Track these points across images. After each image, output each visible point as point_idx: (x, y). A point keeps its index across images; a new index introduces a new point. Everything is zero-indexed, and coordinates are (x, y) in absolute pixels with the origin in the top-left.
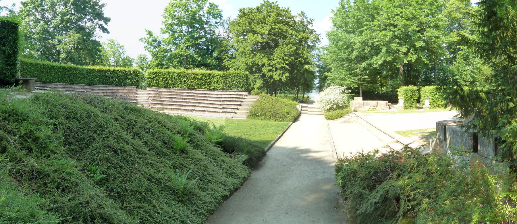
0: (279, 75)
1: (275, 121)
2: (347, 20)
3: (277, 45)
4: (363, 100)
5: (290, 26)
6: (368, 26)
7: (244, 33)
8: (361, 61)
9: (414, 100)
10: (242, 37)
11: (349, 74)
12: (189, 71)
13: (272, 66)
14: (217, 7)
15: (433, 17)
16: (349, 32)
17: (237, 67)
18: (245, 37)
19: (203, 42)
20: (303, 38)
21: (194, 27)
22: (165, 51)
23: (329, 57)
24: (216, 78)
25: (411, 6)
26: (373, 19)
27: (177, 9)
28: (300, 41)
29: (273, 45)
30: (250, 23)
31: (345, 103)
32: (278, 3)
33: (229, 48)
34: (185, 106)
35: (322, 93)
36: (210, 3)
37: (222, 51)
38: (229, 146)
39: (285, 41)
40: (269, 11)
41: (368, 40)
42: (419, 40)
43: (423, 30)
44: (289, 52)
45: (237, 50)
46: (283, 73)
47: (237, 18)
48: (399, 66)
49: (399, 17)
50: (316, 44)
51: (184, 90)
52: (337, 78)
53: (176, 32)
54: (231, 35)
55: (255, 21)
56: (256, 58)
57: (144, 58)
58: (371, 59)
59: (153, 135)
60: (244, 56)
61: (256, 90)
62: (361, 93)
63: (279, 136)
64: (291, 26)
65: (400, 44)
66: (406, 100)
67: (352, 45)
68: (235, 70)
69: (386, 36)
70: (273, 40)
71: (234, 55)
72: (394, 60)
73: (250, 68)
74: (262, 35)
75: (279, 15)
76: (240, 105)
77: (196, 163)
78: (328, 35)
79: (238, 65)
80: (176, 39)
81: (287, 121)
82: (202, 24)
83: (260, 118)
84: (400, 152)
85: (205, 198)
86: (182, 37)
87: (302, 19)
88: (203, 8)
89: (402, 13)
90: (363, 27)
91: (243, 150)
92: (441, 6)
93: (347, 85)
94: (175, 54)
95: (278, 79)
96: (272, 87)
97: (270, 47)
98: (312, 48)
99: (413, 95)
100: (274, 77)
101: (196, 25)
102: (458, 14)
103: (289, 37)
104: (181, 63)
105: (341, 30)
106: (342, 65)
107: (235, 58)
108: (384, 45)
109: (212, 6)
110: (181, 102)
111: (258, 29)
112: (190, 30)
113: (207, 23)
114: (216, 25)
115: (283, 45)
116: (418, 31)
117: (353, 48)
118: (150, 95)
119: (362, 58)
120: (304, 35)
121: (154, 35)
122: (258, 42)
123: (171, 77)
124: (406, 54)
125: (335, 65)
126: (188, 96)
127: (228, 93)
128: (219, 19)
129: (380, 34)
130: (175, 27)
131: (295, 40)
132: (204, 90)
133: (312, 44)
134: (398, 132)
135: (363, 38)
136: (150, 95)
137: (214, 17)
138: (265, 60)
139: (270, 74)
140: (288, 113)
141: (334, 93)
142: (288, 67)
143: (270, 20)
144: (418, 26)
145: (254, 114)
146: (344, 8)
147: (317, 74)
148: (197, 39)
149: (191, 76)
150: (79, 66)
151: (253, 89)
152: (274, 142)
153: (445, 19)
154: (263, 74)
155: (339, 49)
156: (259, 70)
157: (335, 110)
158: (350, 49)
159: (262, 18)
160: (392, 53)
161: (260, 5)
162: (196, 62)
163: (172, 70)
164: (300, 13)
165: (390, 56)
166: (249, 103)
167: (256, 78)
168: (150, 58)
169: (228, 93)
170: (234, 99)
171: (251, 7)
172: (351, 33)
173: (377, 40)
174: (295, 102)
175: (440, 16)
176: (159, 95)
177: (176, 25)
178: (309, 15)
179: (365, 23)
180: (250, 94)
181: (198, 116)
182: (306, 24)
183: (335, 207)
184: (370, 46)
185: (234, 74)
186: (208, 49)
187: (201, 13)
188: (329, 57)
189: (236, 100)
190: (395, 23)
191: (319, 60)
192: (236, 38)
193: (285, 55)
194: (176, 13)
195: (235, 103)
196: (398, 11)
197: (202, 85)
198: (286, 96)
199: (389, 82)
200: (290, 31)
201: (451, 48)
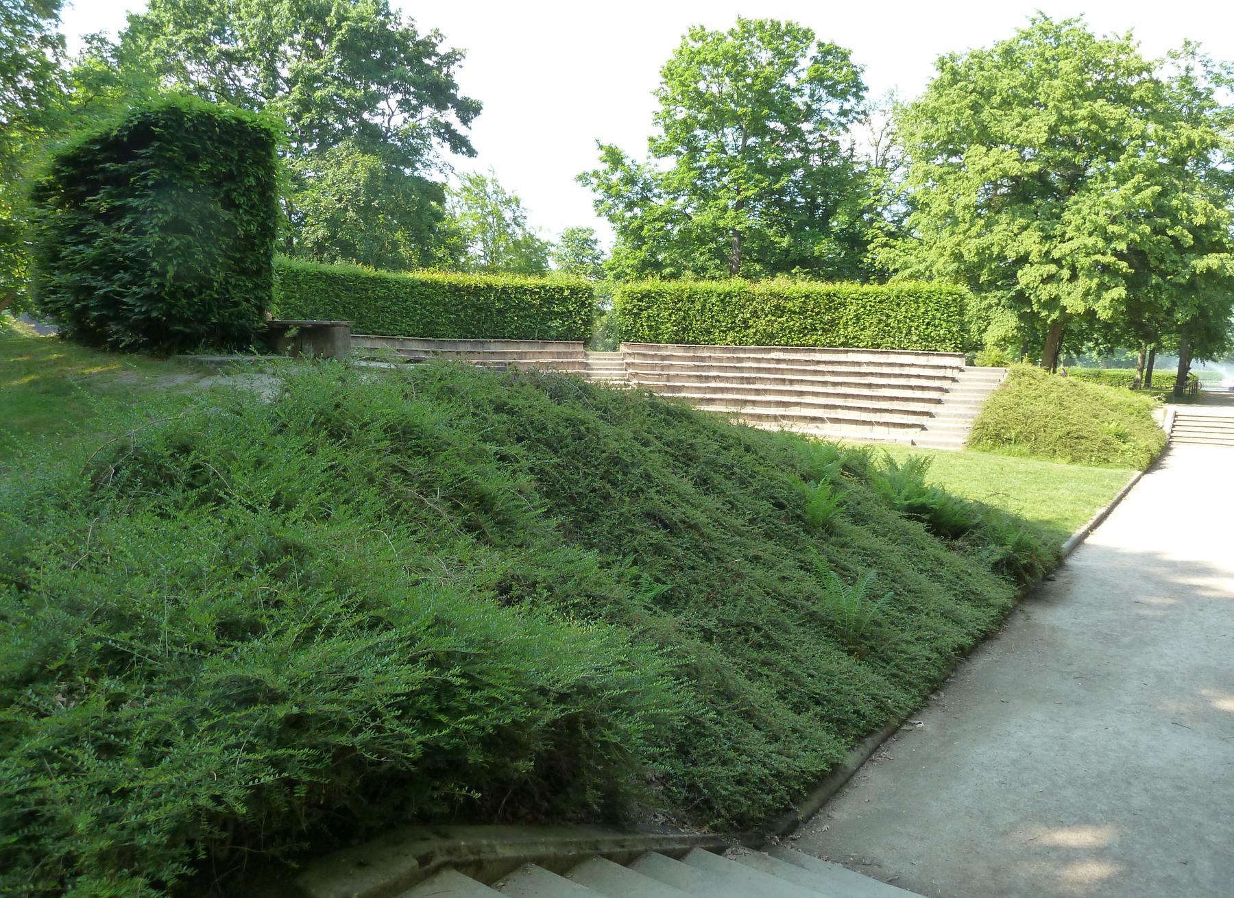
0: (1086, 294)
1: (1074, 461)
3: (1076, 181)
7: (952, 146)
12: (763, 286)
13: (1058, 262)
14: (845, 57)
22: (668, 217)
24: (853, 308)
30: (976, 108)
32: (1084, 19)
34: (754, 403)
36: (821, 45)
38: (948, 523)
46: (1103, 287)
51: (745, 351)
56: (997, 236)
57: (586, 240)
59: (743, 483)
63: (1100, 511)
64: (1141, 102)
75: (1090, 63)
76: (939, 402)
79: (924, 261)
80: (701, 176)
81: (1123, 465)
83: (1016, 448)
85: (912, 649)
86: (725, 167)
87: (1188, 69)
88: (795, 64)
94: (703, 227)
95: (1081, 310)
100: (1065, 301)
101: (772, 125)
104: (724, 259)
109: (828, 52)
110: (738, 391)
111: (1006, 126)
113: (809, 113)
114: (843, 120)
115: (1105, 180)
118: (630, 371)
120: (1196, 135)
121: (627, 162)
123: (698, 306)
126: (759, 370)
127: (781, 355)
128: (853, 101)
130: (699, 132)
136: (630, 371)
137: (833, 92)
138: (1030, 242)
139: (1046, 292)
140: (1122, 437)
142: (1123, 265)
145: (992, 435)
148: (776, 173)
149: (766, 301)
150: (383, 273)
151: (978, 346)
159: (1023, 85)
161: (1015, 35)
164: (1178, 47)
166: (972, 397)
167: (990, 306)
168: (607, 239)
169: (893, 358)
170: (914, 382)
174: (1144, 398)
176: (663, 368)
177: (703, 127)
182: (1201, 84)
185: (915, 296)
193: (1114, 220)
194: (702, 86)
197: (803, 331)
200: (1137, 126)
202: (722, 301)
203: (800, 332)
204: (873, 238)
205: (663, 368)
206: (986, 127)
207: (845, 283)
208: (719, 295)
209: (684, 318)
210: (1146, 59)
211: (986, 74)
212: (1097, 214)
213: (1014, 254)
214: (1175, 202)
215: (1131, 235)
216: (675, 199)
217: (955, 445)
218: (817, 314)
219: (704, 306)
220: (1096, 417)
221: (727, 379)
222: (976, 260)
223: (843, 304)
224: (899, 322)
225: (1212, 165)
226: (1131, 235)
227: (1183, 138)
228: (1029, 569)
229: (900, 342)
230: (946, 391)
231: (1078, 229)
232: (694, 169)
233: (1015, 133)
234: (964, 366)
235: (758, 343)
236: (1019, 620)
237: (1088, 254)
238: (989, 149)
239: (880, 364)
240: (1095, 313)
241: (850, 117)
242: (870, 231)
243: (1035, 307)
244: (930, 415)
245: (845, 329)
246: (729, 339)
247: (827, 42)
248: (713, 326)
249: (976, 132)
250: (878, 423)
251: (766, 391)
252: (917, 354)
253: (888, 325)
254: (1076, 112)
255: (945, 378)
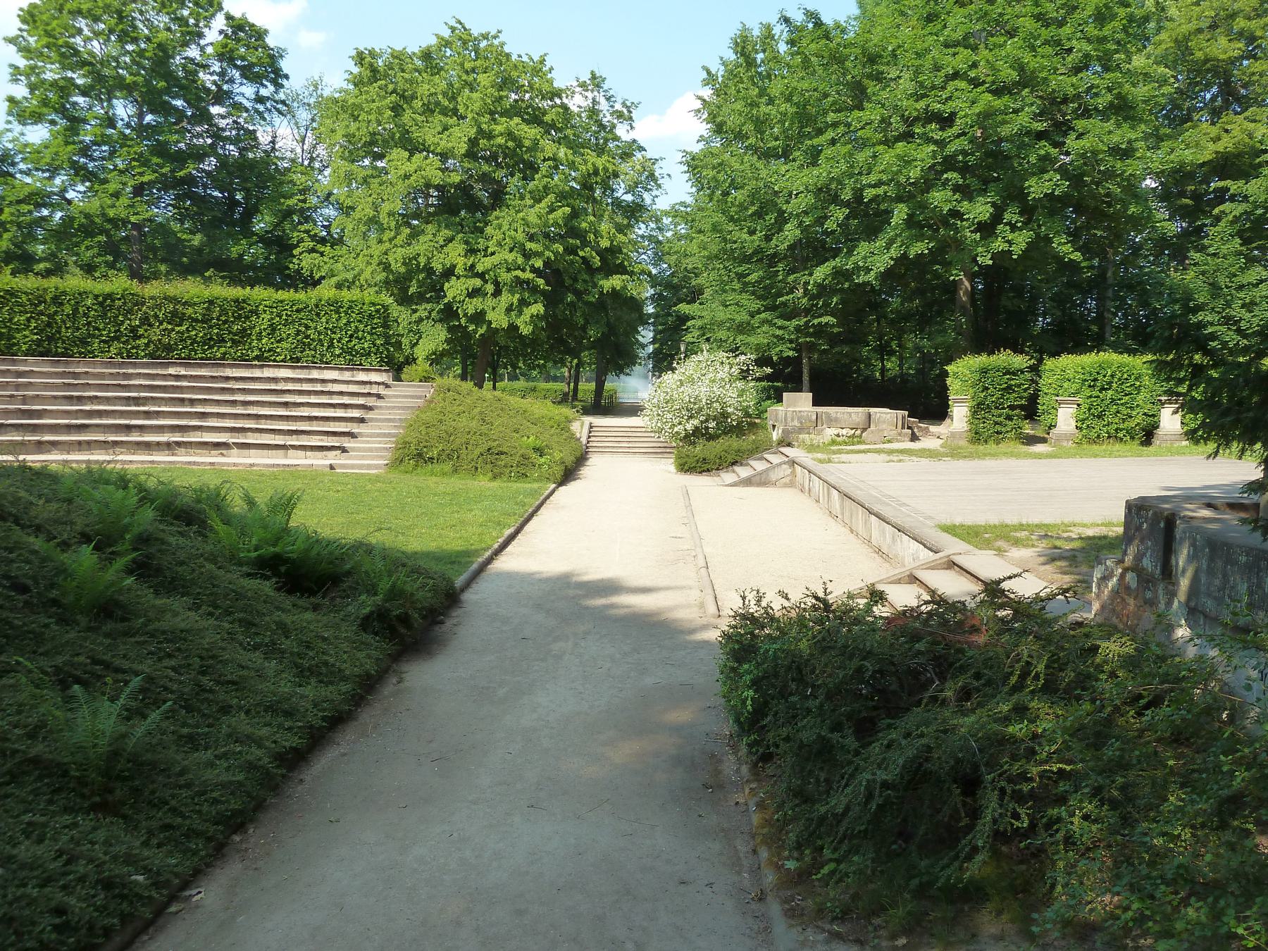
0: (509, 310)
2: (764, 109)
3: (498, 197)
4: (815, 404)
5: (548, 127)
6: (841, 129)
7: (374, 147)
8: (807, 259)
9: (1012, 408)
10: (367, 162)
11: (767, 309)
12: (152, 289)
13: (482, 276)
15: (1107, 69)
16: (767, 155)
17: (350, 276)
18: (379, 164)
19: (209, 173)
20: (596, 173)
21: (166, 109)
22: (38, 199)
23: (693, 247)
25: (1011, 34)
26: (859, 96)
27: (82, 23)
28: (587, 186)
29: (484, 196)
31: (747, 415)
32: (502, 38)
33: (313, 200)
35: (668, 377)
36: (229, 17)
37: (288, 213)
38: (308, 573)
39: (532, 185)
40: (468, 65)
41: (840, 182)
42: (1044, 171)
43: (1063, 128)
44: (546, 225)
45: (346, 210)
46: (523, 303)
47: (345, 85)
48: (957, 275)
49: (962, 84)
50: (646, 196)
51: (135, 365)
52: (721, 324)
53: (85, 121)
54: (321, 151)
55: (417, 104)
56: (422, 246)
58: (850, 252)
60: (373, 236)
61: (422, 366)
62: (806, 378)
63: (508, 532)
64: (553, 126)
65: (965, 192)
66: (979, 409)
67: (780, 201)
68: (339, 286)
69: (909, 162)
70: (484, 178)
71: (335, 231)
72: (937, 255)
73: (396, 281)
74: (444, 156)
75: (507, 83)
76: (362, 420)
77: (169, 648)
78: (694, 165)
79: (353, 270)
81: (539, 480)
82: (200, 99)
83: (437, 468)
84: (971, 604)
85: (209, 775)
89: (975, 65)
90: (820, 132)
91: (374, 586)
92: (1146, 19)
93: (758, 348)
94: (87, 216)
95: (505, 325)
96: (481, 355)
97: (474, 205)
98: (635, 211)
99: (1009, 389)
100: (490, 316)
102: (1223, 41)
103: (544, 167)
104: (117, 255)
105: (738, 148)
106: (741, 276)
107: (340, 241)
108: (899, 199)
110: (122, 414)
111: (429, 134)
112: (149, 118)
113: (221, 97)
114: (261, 108)
115: (522, 198)
116: (1040, 136)
117: (781, 212)
119: (815, 249)
120: (600, 162)
122: (428, 185)
123: (68, 310)
124: (987, 229)
125: (713, 275)
127: (315, 374)
128: (272, 88)
129: (888, 157)
131: (567, 179)
132: (220, 362)
133: (629, 198)
134: (951, 530)
135: (819, 174)
137: (249, 74)
138: (455, 254)
139: (472, 306)
140: (540, 451)
141: (709, 378)
142: (541, 281)
143: (471, 102)
144: (1041, 115)
145: (414, 454)
146: (750, 63)
147: (650, 309)
149: (159, 307)
151: (411, 360)
152: (488, 554)
153: (1161, 69)
154: (449, 306)
155: (732, 219)
156: (433, 289)
157: (711, 438)
158: (771, 218)
160: (930, 227)
161: (433, 41)
162: (184, 254)
163: (75, 281)
164: (586, 77)
165: (920, 238)
166: (397, 415)
167: (421, 320)
169: (315, 374)
171: (398, 48)
172: (778, 157)
173: (873, 178)
174: (566, 411)
175: (1138, 61)
176: (18, 387)
177: (84, 94)
178: (621, 87)
179: (831, 117)
180: (398, 378)
181: (184, 466)
182: (607, 119)
183: (706, 786)
184: (847, 204)
185: (336, 305)
186: (234, 203)
187: (193, 52)
188: (693, 247)
189: (346, 400)
190: (947, 109)
191: (658, 259)
192: (344, 166)
193: (531, 238)
194: (78, 40)
195: (340, 413)
196: (961, 59)
197: (209, 342)
198: (534, 390)
199: (911, 340)
200: (548, 147)
201: (1182, 194)
202: (101, 304)
203: (205, 344)
204: (299, 242)
205: (18, 387)
206: (408, 132)
207: (256, 288)
208: (96, 297)
209: (49, 325)
210: (558, 84)
211: (406, 76)
212: (516, 231)
213: (440, 266)
214: (584, 225)
215: (547, 253)
216: (51, 178)
217: (376, 467)
218: (225, 322)
219: (75, 311)
220: (516, 431)
221: (108, 400)
222: (403, 270)
223: (255, 312)
224: (320, 333)
225: (616, 195)
226: (547, 253)
227: (590, 166)
228: (405, 620)
229: (323, 356)
230: (371, 409)
231: (499, 244)
232: (74, 143)
233: (436, 140)
234: (390, 382)
235: (152, 356)
236: (388, 688)
237: (509, 270)
238: (412, 155)
239: (300, 380)
240: (517, 328)
241: (268, 105)
242: (295, 234)
243: (463, 321)
244: (352, 435)
245: (260, 340)
246: (113, 350)
247: (237, 15)
248: (90, 336)
249: (398, 135)
250: (294, 447)
251: (158, 414)
252: (341, 369)
253: (307, 337)
254: (494, 127)
255: (369, 394)
